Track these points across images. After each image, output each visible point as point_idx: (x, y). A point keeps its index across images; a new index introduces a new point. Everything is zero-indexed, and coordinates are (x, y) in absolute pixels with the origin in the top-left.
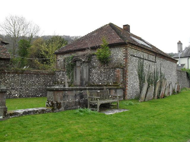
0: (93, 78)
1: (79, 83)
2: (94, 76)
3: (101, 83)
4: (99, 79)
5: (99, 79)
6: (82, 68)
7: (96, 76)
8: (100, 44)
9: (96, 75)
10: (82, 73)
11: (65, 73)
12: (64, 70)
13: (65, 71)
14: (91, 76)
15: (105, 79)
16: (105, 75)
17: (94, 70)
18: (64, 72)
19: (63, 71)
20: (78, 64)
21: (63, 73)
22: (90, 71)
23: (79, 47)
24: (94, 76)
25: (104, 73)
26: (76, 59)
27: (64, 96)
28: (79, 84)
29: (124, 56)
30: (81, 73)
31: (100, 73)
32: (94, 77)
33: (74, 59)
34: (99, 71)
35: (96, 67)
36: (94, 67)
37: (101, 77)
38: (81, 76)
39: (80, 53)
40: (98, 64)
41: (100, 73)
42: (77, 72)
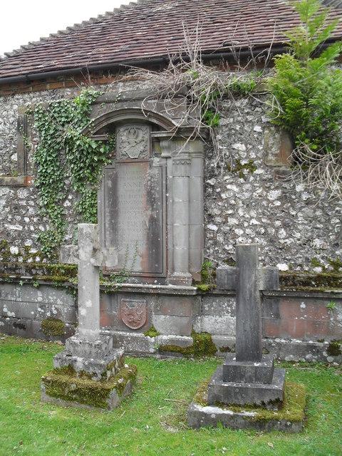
0: (230, 235)
1: (139, 259)
2: (232, 221)
3: (285, 260)
4: (272, 241)
5: (272, 241)
6: (163, 169)
7: (254, 222)
8: (289, 37)
9: (253, 213)
10: (156, 198)
11: (28, 199)
12: (20, 180)
13: (25, 186)
14: (218, 220)
15: (318, 243)
16: (315, 218)
17: (239, 185)
18: (23, 194)
19: (16, 186)
20: (131, 143)
21: (16, 197)
22: (210, 194)
23: (102, 55)
24: (232, 221)
25: (308, 203)
26: (123, 111)
27: (212, 217)
28: (138, 268)
29: (171, 326)
30: (151, 200)
31: (278, 203)
32: (240, 226)
33: (108, 116)
34: (274, 194)
35: (251, 166)
36: (239, 167)
37: (285, 226)
38: (153, 220)
39: (150, 81)
40: (267, 149)
41: (278, 203)
42: (123, 190)
